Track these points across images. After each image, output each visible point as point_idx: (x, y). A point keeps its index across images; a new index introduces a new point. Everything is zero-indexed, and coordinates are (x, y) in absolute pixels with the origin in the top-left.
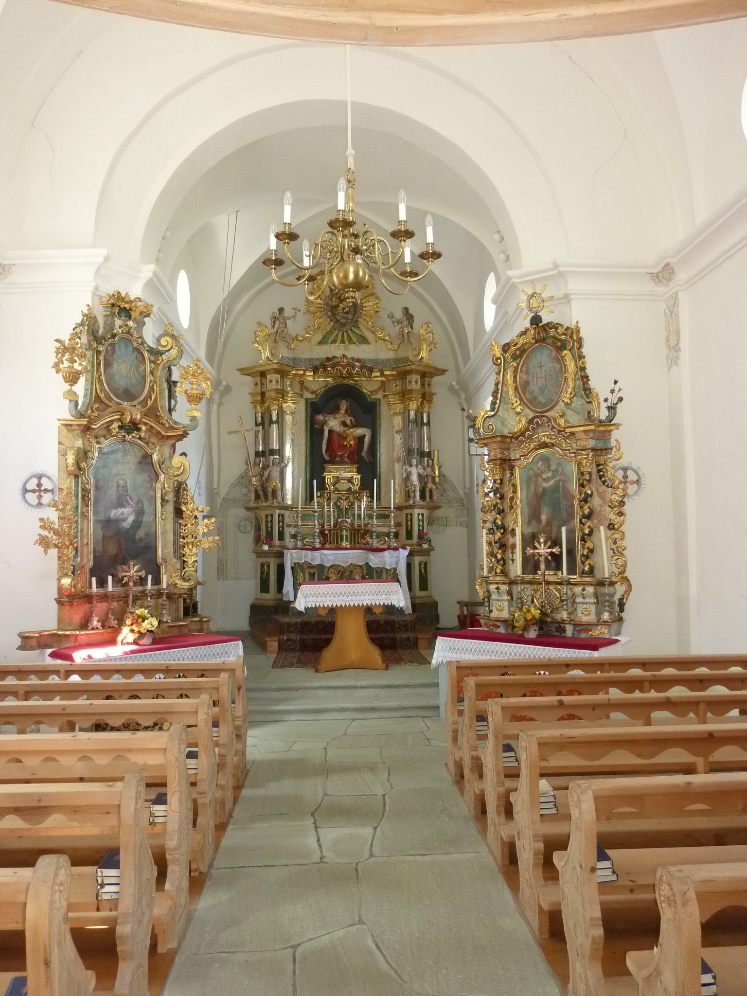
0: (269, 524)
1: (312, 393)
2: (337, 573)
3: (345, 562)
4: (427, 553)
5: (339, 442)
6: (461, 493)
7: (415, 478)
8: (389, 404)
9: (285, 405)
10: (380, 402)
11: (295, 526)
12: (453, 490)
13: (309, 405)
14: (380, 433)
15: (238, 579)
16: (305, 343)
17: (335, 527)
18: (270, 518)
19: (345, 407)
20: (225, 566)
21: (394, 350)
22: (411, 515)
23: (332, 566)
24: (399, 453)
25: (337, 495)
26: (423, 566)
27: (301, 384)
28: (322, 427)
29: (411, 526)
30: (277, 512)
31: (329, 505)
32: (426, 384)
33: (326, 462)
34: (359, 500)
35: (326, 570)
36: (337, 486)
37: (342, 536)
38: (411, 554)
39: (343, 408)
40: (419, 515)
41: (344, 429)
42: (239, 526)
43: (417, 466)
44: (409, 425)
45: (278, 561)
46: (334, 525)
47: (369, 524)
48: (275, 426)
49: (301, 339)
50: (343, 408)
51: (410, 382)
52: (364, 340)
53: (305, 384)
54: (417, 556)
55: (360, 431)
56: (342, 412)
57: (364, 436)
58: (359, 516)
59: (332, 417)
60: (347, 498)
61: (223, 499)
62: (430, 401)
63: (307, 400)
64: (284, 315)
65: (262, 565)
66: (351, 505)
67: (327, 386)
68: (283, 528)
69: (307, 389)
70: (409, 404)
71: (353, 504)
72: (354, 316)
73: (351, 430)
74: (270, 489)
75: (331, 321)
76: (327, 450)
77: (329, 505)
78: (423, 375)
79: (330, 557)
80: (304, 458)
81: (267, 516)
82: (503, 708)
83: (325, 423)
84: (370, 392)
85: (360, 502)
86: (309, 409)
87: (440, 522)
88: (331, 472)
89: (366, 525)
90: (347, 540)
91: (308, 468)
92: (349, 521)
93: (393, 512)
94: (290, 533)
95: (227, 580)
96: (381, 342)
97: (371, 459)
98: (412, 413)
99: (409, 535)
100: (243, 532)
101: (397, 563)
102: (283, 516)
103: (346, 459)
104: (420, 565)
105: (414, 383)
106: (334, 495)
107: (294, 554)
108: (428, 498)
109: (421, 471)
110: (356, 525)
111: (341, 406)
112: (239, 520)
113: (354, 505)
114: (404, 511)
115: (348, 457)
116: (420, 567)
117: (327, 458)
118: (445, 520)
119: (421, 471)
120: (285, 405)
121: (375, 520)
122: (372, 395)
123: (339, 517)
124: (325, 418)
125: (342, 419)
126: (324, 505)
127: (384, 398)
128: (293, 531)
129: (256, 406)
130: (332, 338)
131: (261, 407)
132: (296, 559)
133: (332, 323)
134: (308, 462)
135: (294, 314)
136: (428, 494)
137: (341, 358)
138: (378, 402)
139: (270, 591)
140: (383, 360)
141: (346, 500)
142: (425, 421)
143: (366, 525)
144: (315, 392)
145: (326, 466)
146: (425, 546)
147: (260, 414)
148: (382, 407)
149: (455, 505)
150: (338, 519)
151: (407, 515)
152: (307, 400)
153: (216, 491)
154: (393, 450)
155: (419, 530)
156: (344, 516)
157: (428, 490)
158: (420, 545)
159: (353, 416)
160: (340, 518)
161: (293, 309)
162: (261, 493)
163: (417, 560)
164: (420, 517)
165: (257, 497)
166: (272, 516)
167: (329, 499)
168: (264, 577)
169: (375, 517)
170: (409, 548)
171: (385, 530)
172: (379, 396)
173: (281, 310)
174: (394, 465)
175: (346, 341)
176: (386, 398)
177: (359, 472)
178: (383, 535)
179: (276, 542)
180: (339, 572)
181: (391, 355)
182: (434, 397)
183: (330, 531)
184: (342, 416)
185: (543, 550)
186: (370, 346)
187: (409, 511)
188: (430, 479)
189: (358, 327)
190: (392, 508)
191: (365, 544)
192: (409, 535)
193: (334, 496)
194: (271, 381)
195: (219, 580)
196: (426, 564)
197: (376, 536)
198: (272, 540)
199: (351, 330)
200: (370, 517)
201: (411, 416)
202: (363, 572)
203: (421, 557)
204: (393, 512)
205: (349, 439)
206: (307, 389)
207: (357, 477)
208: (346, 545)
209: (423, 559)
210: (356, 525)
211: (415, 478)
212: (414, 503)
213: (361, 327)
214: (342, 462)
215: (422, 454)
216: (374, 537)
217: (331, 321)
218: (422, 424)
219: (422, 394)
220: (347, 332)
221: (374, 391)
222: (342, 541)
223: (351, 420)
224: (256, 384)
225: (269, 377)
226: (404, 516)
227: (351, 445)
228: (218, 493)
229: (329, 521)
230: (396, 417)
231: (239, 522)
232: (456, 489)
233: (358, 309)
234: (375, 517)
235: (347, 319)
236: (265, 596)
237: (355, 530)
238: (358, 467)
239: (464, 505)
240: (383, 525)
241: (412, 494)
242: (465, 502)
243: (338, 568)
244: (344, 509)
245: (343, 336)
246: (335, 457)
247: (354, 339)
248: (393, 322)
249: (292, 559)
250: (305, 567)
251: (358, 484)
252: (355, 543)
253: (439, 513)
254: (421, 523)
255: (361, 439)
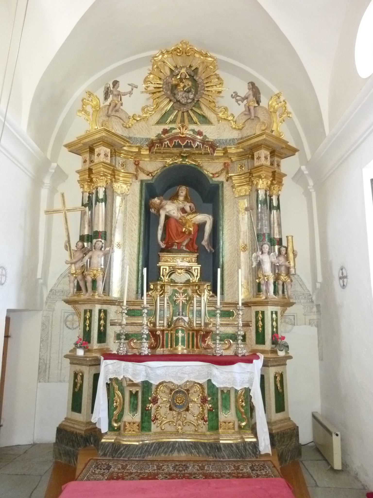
0: (88, 322)
1: (148, 175)
2: (168, 391)
3: (180, 378)
4: (282, 362)
5: (177, 230)
6: (309, 287)
7: (267, 267)
8: (233, 187)
9: (115, 185)
10: (223, 185)
11: (120, 325)
12: (301, 285)
13: (144, 187)
14: (223, 218)
15: (60, 381)
16: (143, 123)
17: (169, 326)
18: (88, 314)
19: (184, 193)
20: (48, 366)
21: (239, 129)
22: (263, 313)
23: (160, 384)
24: (245, 241)
25: (172, 288)
26: (278, 378)
27: (136, 165)
28: (158, 211)
29: (263, 327)
30: (98, 307)
31: (162, 300)
32: (276, 164)
33: (163, 250)
34: (198, 294)
35: (153, 388)
36: (173, 277)
37: (177, 338)
38: (265, 365)
39: (182, 194)
40: (272, 313)
41: (183, 215)
42: (65, 322)
43: (269, 253)
44: (258, 206)
45: (93, 371)
46: (168, 324)
47: (210, 324)
48: (102, 206)
49: (138, 119)
50: (182, 194)
51: (259, 158)
52: (205, 120)
53: (140, 165)
54: (271, 366)
55: (200, 218)
56: (181, 198)
57: (204, 224)
58: (199, 312)
59: (169, 202)
60: (185, 291)
61: (51, 290)
62: (280, 183)
63: (142, 181)
64: (118, 89)
65: (76, 375)
66: (189, 300)
67: (165, 166)
68: (105, 326)
69: (143, 171)
70: (257, 184)
71: (191, 299)
72: (195, 95)
73: (191, 216)
74: (89, 279)
75: (170, 101)
76: (163, 239)
77: (162, 300)
78: (273, 153)
79: (158, 372)
80: (136, 245)
81: (85, 311)
82: (94, 162)
83: (160, 208)
84: (212, 174)
85: (200, 296)
86: (144, 191)
87: (287, 320)
88: (167, 261)
89: (206, 324)
90: (183, 344)
91: (141, 256)
92: (186, 319)
93: (242, 310)
94: (115, 332)
95: (48, 382)
96: (224, 122)
97: (212, 249)
98: (261, 194)
99: (260, 339)
100: (69, 328)
101: (251, 381)
102: (105, 312)
103: (184, 248)
104: (275, 377)
105: (263, 159)
106: (169, 287)
107: (110, 367)
108: (280, 292)
109: (274, 260)
110: (195, 325)
111: (180, 192)
112: (66, 314)
113: (193, 300)
114: (253, 307)
115: (187, 246)
116: (275, 381)
117: (163, 246)
118: (292, 318)
119: (274, 260)
120: (115, 185)
121: (218, 319)
122: (214, 177)
123: (174, 314)
124: (161, 201)
125: (181, 206)
126: (156, 300)
127: (227, 181)
128: (117, 329)
129: (83, 185)
130: (172, 117)
131: (89, 186)
132: (113, 373)
133: (171, 104)
134: (141, 250)
135: (131, 90)
136: (280, 288)
137: (180, 129)
138: (220, 185)
139: (82, 411)
140: (226, 140)
141: (183, 293)
142: (275, 203)
143: (206, 324)
144: (151, 173)
145: (161, 254)
146: (281, 354)
147: (88, 194)
148: (225, 190)
149: (302, 301)
150: (173, 316)
151: (257, 313)
152: (142, 181)
153: (41, 281)
154: (238, 237)
155: (273, 332)
156: (181, 314)
157: (281, 282)
158: (274, 352)
159: (192, 203)
160: (175, 316)
161: (129, 85)
162: (82, 284)
163: (272, 371)
164: (274, 316)
165: (79, 288)
166: (91, 311)
167: (163, 292)
168: (76, 390)
169: (218, 315)
170: (262, 356)
171: (230, 330)
172: (222, 178)
173: (115, 83)
174: (239, 255)
175: (186, 120)
176: (230, 181)
177: (198, 261)
178: (227, 337)
179: (95, 344)
180: (171, 390)
181: (235, 135)
182: (284, 179)
183: (163, 331)
184: (181, 202)
185: (181, 299)
186: (212, 127)
187: (260, 309)
188: (283, 269)
189: (200, 108)
190: (240, 304)
191: (205, 349)
192: (260, 339)
193: (169, 289)
194: (99, 155)
195: (40, 382)
196: (282, 375)
197: (221, 340)
198: (89, 342)
199: (192, 110)
200: (213, 314)
201: (260, 197)
202: (203, 391)
203: (279, 367)
204: (242, 310)
205: (187, 225)
206: (143, 171)
207: (196, 268)
208: (183, 349)
209: (279, 369)
210: (195, 325)
211: (267, 267)
212: (266, 298)
213: (203, 107)
214: (180, 251)
215: (272, 242)
216: (218, 342)
217: (170, 101)
218: (271, 208)
219: (272, 172)
220: (188, 111)
221: (216, 173)
222: (177, 344)
223: (190, 207)
224: (85, 162)
225: (97, 150)
226: (254, 314)
227: (190, 232)
228: (45, 283)
229: (162, 318)
230: (240, 201)
231: (66, 316)
232: (304, 284)
233: (199, 89)
234: (218, 315)
235: (188, 98)
236: (76, 416)
237: (193, 330)
238: (198, 256)
239: (312, 302)
240: (227, 325)
241: (263, 288)
242: (314, 298)
243: (168, 385)
244: (181, 304)
245: (183, 116)
246: (172, 245)
247: (195, 119)
248: (237, 101)
249: (107, 372)
250: (125, 384)
251: (197, 276)
252: (193, 347)
253: (290, 310)
254: (274, 323)
255: (201, 227)
